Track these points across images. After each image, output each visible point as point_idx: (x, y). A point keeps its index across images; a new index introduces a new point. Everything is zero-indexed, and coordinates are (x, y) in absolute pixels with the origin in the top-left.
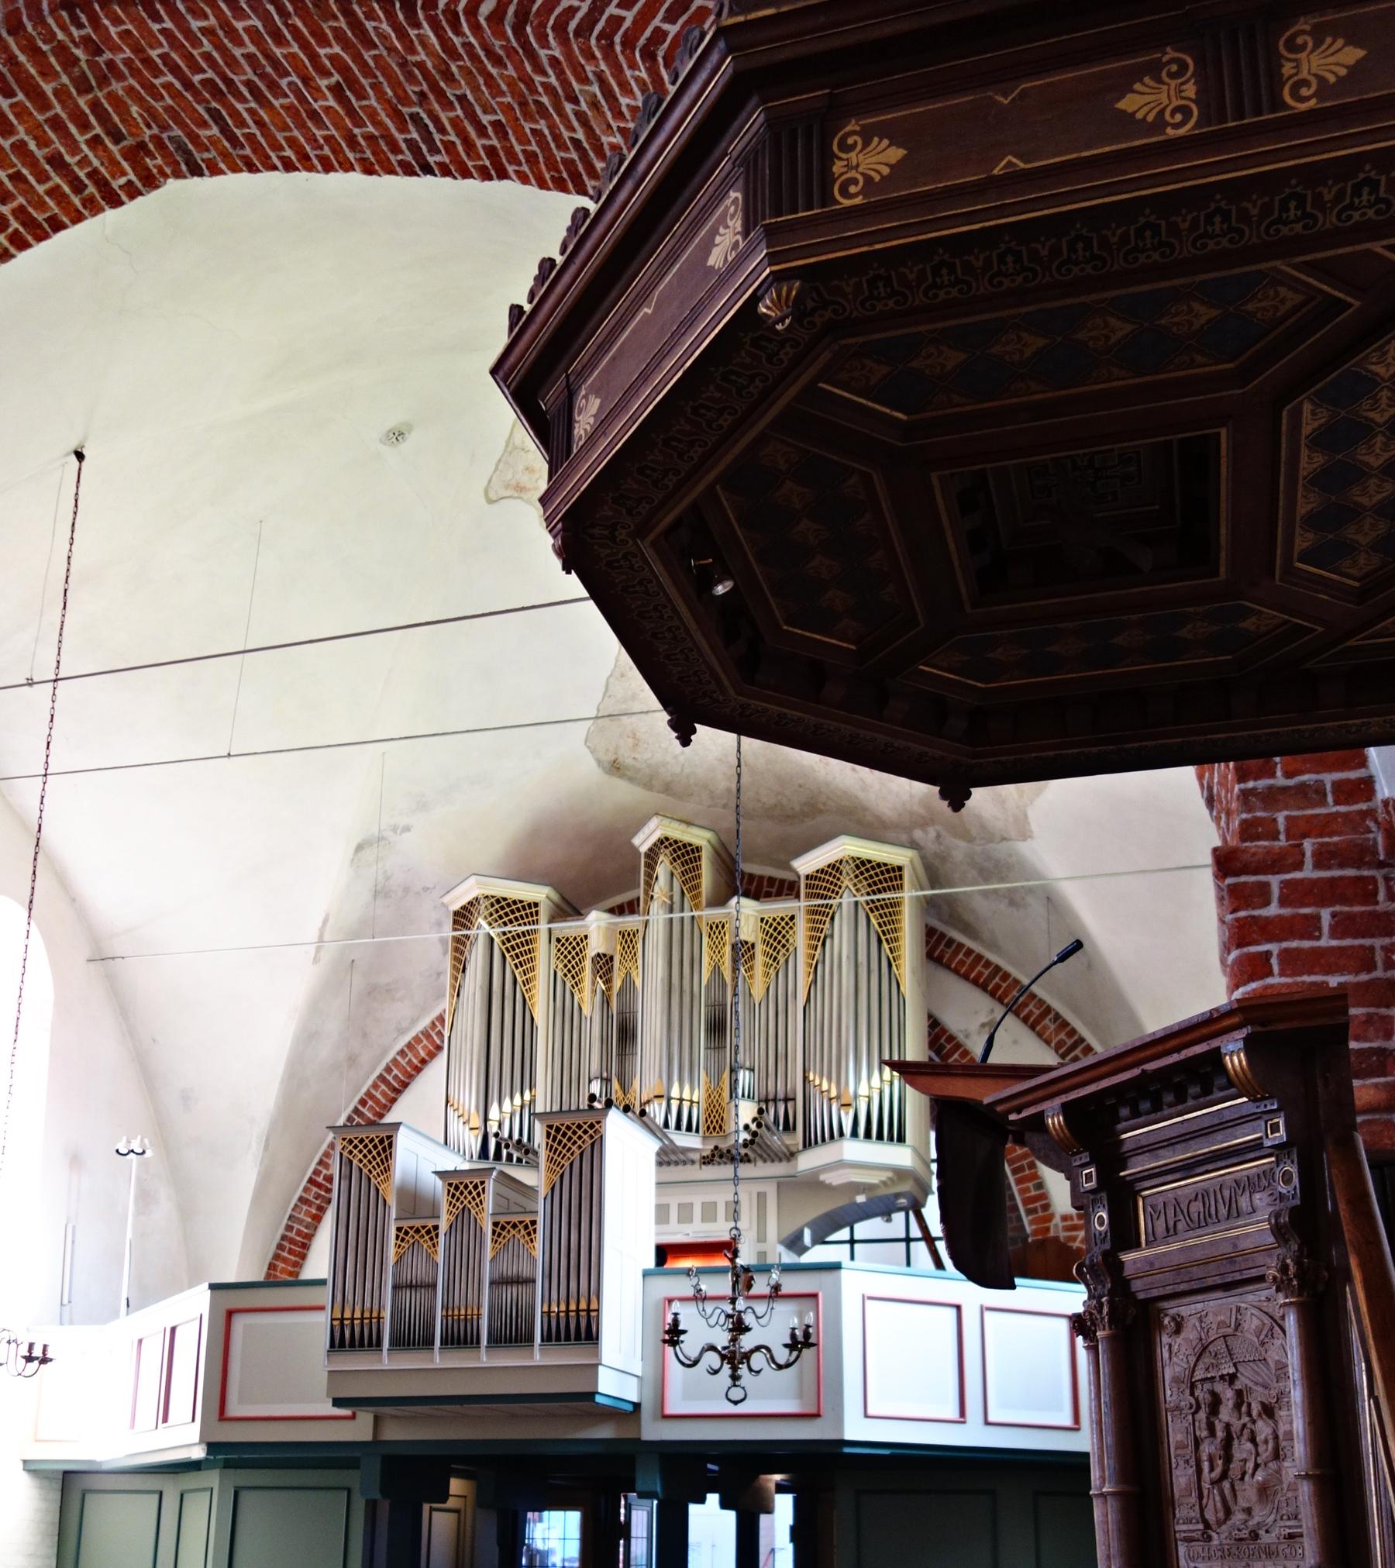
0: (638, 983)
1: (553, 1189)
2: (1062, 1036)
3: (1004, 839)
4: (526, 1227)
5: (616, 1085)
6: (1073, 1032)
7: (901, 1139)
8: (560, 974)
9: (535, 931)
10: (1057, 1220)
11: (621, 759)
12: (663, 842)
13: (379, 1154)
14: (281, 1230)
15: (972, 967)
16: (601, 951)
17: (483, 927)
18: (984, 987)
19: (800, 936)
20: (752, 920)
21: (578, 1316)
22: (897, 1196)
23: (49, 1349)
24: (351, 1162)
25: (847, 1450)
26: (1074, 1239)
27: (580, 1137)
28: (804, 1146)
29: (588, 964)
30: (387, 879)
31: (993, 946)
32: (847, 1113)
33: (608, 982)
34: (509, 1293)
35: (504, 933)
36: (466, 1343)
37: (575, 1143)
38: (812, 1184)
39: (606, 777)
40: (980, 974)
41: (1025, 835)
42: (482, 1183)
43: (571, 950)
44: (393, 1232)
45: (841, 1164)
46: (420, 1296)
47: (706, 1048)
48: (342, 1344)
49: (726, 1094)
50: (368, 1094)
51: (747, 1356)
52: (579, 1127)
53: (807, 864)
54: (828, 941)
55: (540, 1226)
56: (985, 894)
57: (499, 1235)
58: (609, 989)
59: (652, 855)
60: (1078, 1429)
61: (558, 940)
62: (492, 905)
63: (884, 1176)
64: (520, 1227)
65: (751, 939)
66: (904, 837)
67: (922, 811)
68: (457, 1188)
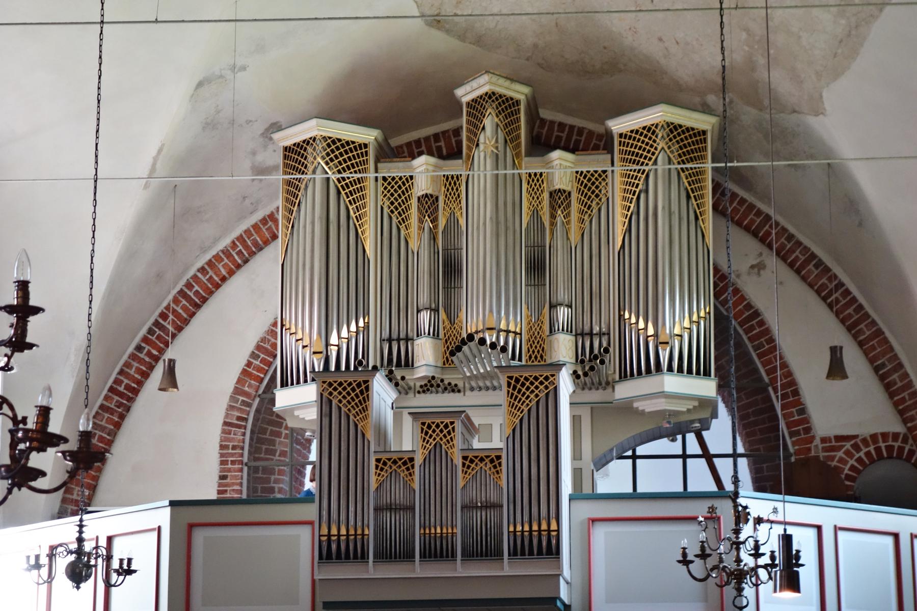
0: (462, 222)
1: (514, 430)
2: (824, 280)
3: (794, 111)
4: (492, 461)
5: (443, 315)
7: (710, 376)
8: (386, 210)
10: (817, 441)
12: (490, 96)
15: (745, 216)
16: (429, 192)
18: (755, 234)
21: (348, 540)
22: (692, 422)
23: (133, 562)
24: (330, 402)
26: (832, 458)
28: (620, 377)
29: (414, 202)
30: (218, 112)
33: (434, 220)
34: (478, 516)
36: (442, 556)
37: (533, 392)
38: (627, 409)
39: (427, 28)
40: (752, 221)
41: (818, 112)
42: (452, 423)
44: (373, 463)
45: (663, 395)
46: (401, 518)
47: (526, 285)
49: (546, 327)
52: (536, 378)
53: (619, 125)
54: (642, 196)
55: (504, 461)
57: (469, 467)
58: (436, 227)
59: (477, 106)
63: (690, 405)
64: (487, 460)
65: (568, 189)
66: (697, 100)
68: (429, 427)
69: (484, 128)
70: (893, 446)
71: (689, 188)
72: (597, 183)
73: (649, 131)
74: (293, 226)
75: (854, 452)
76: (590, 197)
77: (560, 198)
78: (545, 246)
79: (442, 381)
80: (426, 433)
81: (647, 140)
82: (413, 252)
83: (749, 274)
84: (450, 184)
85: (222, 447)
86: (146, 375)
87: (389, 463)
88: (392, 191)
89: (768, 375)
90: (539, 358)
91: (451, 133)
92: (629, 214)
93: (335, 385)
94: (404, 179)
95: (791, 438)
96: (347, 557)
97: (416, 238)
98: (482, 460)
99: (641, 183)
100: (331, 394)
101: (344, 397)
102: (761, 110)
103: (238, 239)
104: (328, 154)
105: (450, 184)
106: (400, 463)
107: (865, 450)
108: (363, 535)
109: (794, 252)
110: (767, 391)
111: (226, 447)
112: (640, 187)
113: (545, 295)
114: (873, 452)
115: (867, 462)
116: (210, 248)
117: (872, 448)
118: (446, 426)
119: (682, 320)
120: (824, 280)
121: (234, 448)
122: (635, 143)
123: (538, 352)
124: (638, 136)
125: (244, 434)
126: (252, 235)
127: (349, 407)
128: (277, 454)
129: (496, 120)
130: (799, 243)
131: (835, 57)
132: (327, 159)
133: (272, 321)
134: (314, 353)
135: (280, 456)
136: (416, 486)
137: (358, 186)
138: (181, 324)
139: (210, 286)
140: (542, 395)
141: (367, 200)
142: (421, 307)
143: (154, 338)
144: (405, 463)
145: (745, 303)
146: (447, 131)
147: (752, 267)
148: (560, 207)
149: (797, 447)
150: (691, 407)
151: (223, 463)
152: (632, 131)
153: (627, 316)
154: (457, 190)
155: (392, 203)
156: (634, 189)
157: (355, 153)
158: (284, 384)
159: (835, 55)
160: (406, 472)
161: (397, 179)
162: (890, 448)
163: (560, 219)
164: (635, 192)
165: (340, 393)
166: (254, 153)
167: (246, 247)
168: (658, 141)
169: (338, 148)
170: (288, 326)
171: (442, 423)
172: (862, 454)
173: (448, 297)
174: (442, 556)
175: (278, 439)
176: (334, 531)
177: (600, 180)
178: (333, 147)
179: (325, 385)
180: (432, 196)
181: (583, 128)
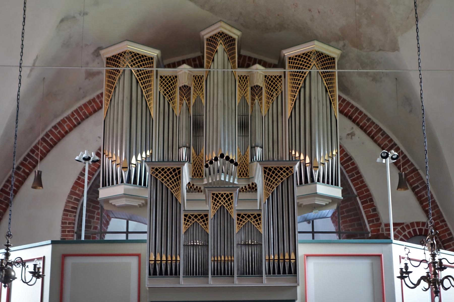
0: (204, 101)
2: (386, 142)
6: (391, 140)
7: (338, 186)
9: (151, 71)
12: (221, 34)
13: (173, 177)
16: (186, 84)
17: (127, 68)
19: (287, 86)
20: (262, 76)
21: (166, 263)
31: (357, 98)
32: (316, 171)
33: (189, 100)
35: (138, 71)
40: (349, 111)
42: (231, 194)
43: (169, 83)
44: (183, 217)
47: (238, 136)
48: (155, 274)
51: (442, 281)
53: (288, 53)
55: (262, 217)
56: (360, 74)
58: (189, 103)
59: (213, 41)
61: (161, 77)
62: (133, 56)
64: (252, 217)
65: (261, 85)
67: (339, 33)
68: (217, 196)
69: (217, 51)
70: (422, 229)
71: (327, 86)
72: (276, 83)
73: (306, 55)
74: (111, 100)
75: (402, 232)
76: (272, 90)
77: (257, 90)
78: (248, 115)
79: (193, 185)
80: (215, 200)
81: (305, 60)
82: (177, 117)
83: (346, 138)
84: (197, 81)
85: (63, 223)
87: (193, 217)
88: (165, 83)
89: (357, 190)
90: (245, 175)
91: (191, 60)
92: (295, 99)
93: (160, 170)
94: (172, 77)
95: (369, 224)
96: (166, 274)
97: (178, 107)
98: (249, 216)
99: (302, 83)
100: (157, 175)
101: (165, 177)
102: (361, 50)
104: (132, 61)
105: (197, 81)
106: (199, 217)
107: (408, 231)
108: (176, 260)
109: (371, 127)
110: (356, 200)
111: (66, 223)
112: (301, 85)
113: (248, 142)
114: (412, 232)
115: (409, 237)
117: (411, 230)
118: (227, 196)
119: (325, 158)
122: (298, 62)
123: (245, 171)
124: (300, 59)
125: (75, 216)
126: (83, 109)
127: (168, 183)
128: (92, 228)
129: (223, 47)
130: (373, 123)
131: (408, 19)
132: (132, 63)
134: (123, 168)
135: (93, 229)
136: (209, 231)
137: (148, 79)
138: (44, 155)
139: (59, 136)
140: (285, 179)
141: (152, 87)
143: (27, 163)
145: (344, 153)
146: (189, 59)
147: (348, 135)
148: (257, 94)
149: (372, 229)
150: (328, 203)
151: (63, 231)
152: (296, 56)
153: (293, 153)
154: (201, 84)
155: (165, 90)
156: (297, 86)
157: (146, 62)
158: (104, 185)
159: (408, 18)
160: (203, 223)
161: (168, 77)
163: (256, 101)
164: (298, 87)
165: (163, 175)
166: (87, 64)
167: (79, 115)
168: (311, 60)
169: (137, 58)
170: (107, 154)
171: (225, 194)
172: (406, 233)
173: (195, 141)
174: (224, 274)
175: (92, 220)
176: (158, 258)
177: (278, 81)
178: (135, 57)
179: (153, 170)
180: (187, 86)
181: (261, 60)
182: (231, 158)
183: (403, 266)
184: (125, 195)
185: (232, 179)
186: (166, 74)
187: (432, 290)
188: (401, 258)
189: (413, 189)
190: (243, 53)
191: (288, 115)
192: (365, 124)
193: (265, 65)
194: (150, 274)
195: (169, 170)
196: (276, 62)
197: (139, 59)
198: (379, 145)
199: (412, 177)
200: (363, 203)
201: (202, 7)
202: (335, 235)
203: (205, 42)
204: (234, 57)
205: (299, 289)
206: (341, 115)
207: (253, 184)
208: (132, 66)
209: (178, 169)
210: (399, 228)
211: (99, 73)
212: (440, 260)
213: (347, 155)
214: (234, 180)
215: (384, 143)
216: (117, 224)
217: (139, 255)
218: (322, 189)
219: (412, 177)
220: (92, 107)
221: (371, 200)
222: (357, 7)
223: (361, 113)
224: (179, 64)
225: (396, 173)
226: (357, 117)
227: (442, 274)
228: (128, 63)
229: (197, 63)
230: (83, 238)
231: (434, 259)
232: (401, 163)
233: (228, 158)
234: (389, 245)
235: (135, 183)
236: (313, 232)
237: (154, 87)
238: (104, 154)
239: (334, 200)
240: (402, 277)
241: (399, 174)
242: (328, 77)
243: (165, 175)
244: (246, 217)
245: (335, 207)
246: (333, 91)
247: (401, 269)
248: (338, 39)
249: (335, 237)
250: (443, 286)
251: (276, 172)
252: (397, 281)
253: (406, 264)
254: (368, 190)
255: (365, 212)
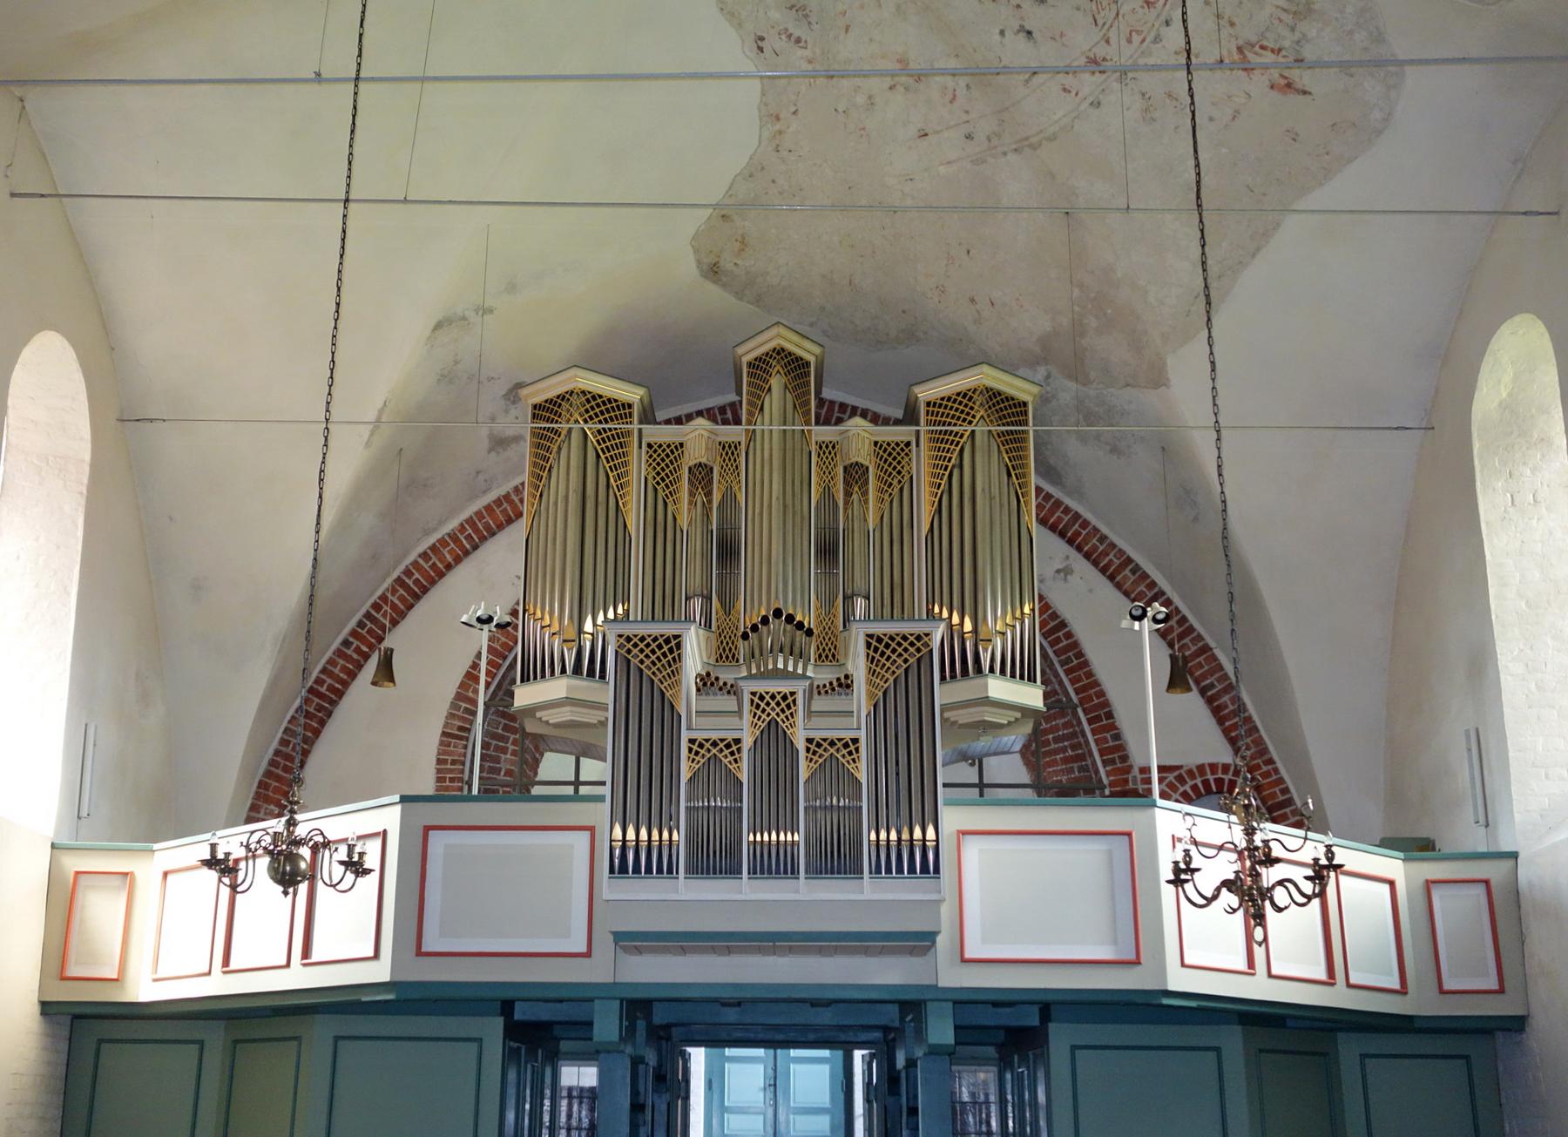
2: (1142, 588)
6: (1153, 584)
11: (722, 263)
12: (780, 351)
13: (664, 655)
14: (275, 744)
16: (704, 460)
17: (574, 424)
18: (1062, 535)
19: (922, 464)
21: (660, 846)
25: (1166, 1001)
27: (906, 650)
30: (456, 363)
32: (985, 650)
33: (709, 494)
40: (1060, 519)
43: (665, 458)
48: (623, 869)
50: (383, 598)
54: (956, 472)
58: (710, 502)
59: (760, 366)
60: (1333, 985)
61: (650, 446)
65: (866, 463)
67: (1037, 349)
68: (762, 698)
80: (758, 706)
85: (439, 761)
86: (353, 675)
87: (707, 745)
97: (685, 511)
101: (647, 656)
103: (467, 521)
107: (1191, 783)
111: (445, 762)
116: (435, 530)
117: (1198, 781)
118: (785, 698)
119: (1005, 624)
120: (1142, 588)
121: (454, 762)
129: (784, 379)
130: (1113, 546)
133: (475, 653)
142: (690, 593)
143: (364, 632)
144: (728, 746)
147: (1058, 571)
151: (439, 780)
153: (937, 609)
158: (525, 679)
160: (731, 758)
162: (1219, 782)
165: (642, 651)
166: (493, 419)
167: (476, 530)
169: (598, 405)
172: (1187, 788)
182: (799, 618)
183: (1179, 856)
184: (569, 701)
185: (800, 665)
186: (660, 440)
187: (1246, 912)
188: (1175, 840)
189: (1203, 692)
190: (827, 394)
191: (925, 528)
192: (1095, 548)
193: (876, 419)
194: (612, 871)
195: (655, 639)
196: (899, 414)
197: (599, 406)
198: (1127, 594)
199: (1200, 665)
200: (1090, 722)
201: (739, 295)
202: (1029, 791)
203: (745, 370)
204: (808, 403)
205: (945, 910)
206: (1042, 528)
207: (847, 677)
208: (586, 421)
209: (676, 637)
210: (1171, 777)
211: (518, 439)
212: (1266, 842)
213: (1055, 616)
214: (805, 669)
215: (1134, 585)
216: (555, 766)
217: (591, 829)
218: (999, 688)
219: (1200, 665)
220: (504, 511)
221: (1110, 715)
222: (1076, 291)
223: (1085, 524)
224: (689, 417)
225: (1165, 652)
226: (1077, 534)
227: (1270, 875)
228: (576, 416)
229: (727, 414)
230: (475, 791)
231: (1250, 841)
232: (1175, 631)
233: (790, 619)
234: (1149, 812)
235: (591, 673)
236: (981, 786)
237: (633, 467)
238: (525, 611)
239: (1026, 711)
240: (1177, 882)
241: (1171, 656)
242: (1013, 443)
243: (647, 651)
244: (825, 745)
245: (1028, 728)
246: (1024, 475)
247: (1176, 863)
248: (1034, 362)
249: (1029, 794)
250: (1273, 904)
251: (894, 645)
252: (1168, 892)
253: (1187, 852)
254: (1102, 694)
255: (1096, 741)
